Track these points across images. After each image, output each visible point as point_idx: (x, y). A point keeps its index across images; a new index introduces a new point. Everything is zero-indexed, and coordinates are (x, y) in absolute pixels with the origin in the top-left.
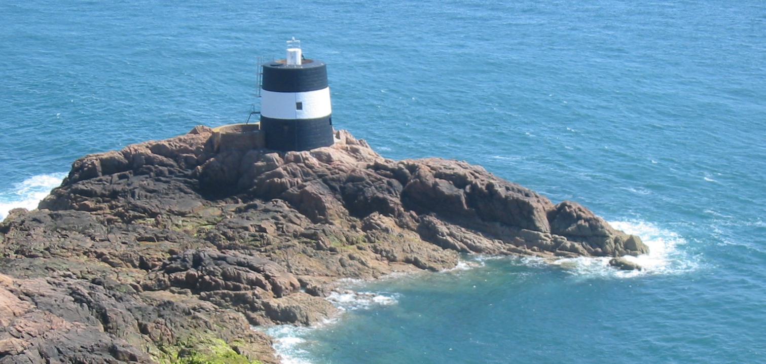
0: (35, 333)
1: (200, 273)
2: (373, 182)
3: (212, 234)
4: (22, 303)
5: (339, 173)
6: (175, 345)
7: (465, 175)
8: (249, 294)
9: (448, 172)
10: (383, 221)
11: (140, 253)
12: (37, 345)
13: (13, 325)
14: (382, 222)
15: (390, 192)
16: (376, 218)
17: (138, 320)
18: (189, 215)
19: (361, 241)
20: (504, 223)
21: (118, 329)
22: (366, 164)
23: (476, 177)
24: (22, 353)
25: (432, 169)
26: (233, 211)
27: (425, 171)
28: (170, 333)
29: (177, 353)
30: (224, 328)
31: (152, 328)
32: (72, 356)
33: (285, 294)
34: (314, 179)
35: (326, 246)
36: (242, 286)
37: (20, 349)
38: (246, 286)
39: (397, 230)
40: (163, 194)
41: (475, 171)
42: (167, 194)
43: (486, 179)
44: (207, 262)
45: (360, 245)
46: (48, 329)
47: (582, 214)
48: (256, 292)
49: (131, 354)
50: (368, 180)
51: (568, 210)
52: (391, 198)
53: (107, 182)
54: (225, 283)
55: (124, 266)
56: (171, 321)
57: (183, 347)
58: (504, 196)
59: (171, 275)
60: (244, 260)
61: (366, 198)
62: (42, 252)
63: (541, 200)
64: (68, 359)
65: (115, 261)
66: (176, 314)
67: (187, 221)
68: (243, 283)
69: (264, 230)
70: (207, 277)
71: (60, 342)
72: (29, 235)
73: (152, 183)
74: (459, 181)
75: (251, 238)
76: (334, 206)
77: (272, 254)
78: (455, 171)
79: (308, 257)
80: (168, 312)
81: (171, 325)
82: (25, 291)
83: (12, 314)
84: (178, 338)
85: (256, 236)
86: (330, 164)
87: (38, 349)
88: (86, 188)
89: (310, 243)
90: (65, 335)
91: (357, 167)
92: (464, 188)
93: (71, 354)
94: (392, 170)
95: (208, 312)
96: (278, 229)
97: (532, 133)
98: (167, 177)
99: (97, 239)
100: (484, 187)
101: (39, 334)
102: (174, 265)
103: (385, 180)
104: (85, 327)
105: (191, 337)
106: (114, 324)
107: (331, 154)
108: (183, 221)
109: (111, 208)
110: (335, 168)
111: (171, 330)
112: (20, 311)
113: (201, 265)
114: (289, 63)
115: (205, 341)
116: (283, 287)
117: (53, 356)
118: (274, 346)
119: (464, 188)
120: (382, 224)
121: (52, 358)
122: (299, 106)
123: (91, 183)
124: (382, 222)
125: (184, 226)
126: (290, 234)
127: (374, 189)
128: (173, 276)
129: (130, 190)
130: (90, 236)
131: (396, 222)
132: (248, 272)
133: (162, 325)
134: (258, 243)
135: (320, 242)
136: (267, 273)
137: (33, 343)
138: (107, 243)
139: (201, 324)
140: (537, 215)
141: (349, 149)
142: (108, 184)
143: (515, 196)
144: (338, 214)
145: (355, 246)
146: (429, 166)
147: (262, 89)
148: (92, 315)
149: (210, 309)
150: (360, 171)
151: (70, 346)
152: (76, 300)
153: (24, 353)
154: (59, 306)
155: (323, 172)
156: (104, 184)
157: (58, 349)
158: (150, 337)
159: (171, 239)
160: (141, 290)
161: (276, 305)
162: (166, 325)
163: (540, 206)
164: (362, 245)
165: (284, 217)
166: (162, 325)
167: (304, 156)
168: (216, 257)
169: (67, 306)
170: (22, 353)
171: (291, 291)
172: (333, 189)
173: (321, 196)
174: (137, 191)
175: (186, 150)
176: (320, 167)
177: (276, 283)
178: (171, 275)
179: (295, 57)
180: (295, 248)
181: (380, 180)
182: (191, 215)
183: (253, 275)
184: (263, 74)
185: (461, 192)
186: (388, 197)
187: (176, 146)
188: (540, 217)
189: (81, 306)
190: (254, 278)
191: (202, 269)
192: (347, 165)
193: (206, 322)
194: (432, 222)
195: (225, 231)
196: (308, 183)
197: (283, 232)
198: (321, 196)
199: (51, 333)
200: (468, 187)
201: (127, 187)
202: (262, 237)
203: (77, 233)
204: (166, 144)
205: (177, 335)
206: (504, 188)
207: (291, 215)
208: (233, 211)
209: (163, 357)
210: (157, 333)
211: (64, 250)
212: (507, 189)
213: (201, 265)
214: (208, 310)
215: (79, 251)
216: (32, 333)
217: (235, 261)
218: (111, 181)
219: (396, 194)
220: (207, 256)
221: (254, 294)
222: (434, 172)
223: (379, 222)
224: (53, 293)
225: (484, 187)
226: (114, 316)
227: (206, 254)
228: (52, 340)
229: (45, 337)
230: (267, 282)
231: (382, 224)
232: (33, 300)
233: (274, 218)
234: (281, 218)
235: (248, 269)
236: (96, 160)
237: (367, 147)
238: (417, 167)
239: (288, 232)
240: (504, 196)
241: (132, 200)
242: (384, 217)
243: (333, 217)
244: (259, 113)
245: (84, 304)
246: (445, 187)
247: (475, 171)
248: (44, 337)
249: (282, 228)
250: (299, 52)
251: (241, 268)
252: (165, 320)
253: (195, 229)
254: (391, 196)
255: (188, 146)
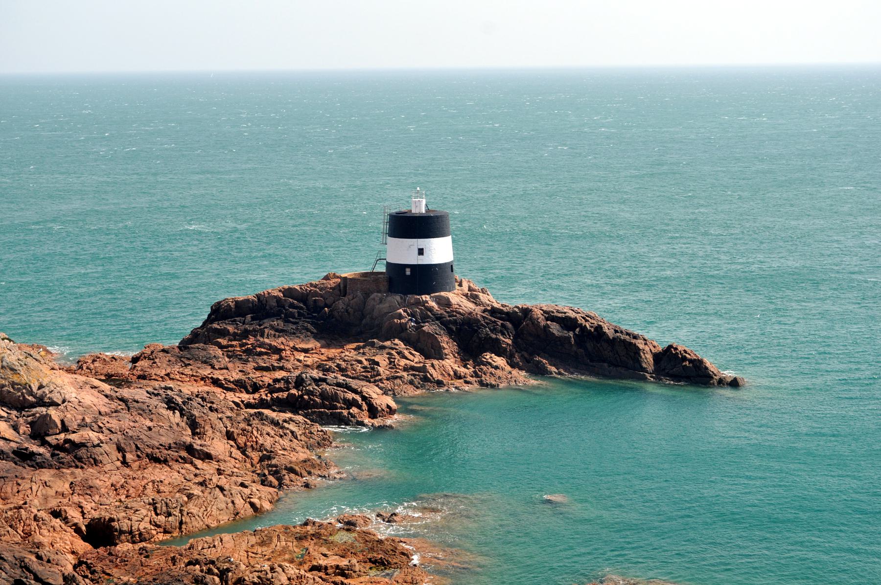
0: (116, 429)
1: (300, 393)
2: (487, 323)
3: (327, 367)
4: (110, 404)
5: (456, 316)
6: (258, 451)
7: (576, 317)
8: (345, 412)
9: (560, 315)
10: (494, 359)
11: (254, 380)
12: (116, 440)
13: (96, 422)
14: (494, 361)
15: (503, 334)
16: (488, 357)
17: (226, 427)
18: (311, 352)
19: (468, 376)
20: (611, 364)
21: (204, 434)
22: (483, 308)
23: (586, 321)
24: (98, 445)
25: (545, 312)
26: (353, 349)
27: (538, 313)
28: (255, 440)
29: (259, 458)
30: (311, 439)
31: (238, 434)
32: (149, 452)
33: (381, 414)
34: (433, 321)
35: (433, 378)
36: (339, 405)
37: (96, 442)
38: (343, 405)
39: (508, 368)
40: (291, 333)
41: (586, 316)
42: (294, 333)
43: (596, 323)
44: (309, 382)
45: (468, 379)
46: (130, 427)
47: (687, 356)
48: (351, 411)
49: (207, 452)
50: (483, 322)
51: (674, 352)
52: (504, 339)
53: (240, 322)
54: (323, 402)
55: (238, 391)
56: (258, 429)
57: (265, 452)
58: (611, 338)
59: (273, 395)
60: (343, 382)
61: (480, 339)
62: (162, 377)
63: (648, 343)
64: (144, 455)
65: (229, 386)
66: (264, 423)
67: (309, 357)
68: (340, 403)
69: (378, 364)
70: (306, 397)
71: (140, 439)
72: (155, 363)
73: (281, 323)
74: (568, 323)
75: (362, 370)
76: (449, 346)
77: (380, 384)
78: (567, 314)
79: (415, 388)
80: (257, 422)
81: (258, 433)
82: (120, 397)
83: (98, 413)
84: (262, 445)
85: (367, 368)
86: (449, 308)
87: (116, 444)
88: (219, 327)
89: (418, 375)
90: (146, 433)
91: (474, 310)
92: (574, 331)
93: (149, 451)
94: (508, 314)
95: (297, 423)
96: (391, 363)
97: (454, 110)
98: (296, 319)
99: (217, 367)
100: (592, 330)
101: (120, 431)
102: (277, 386)
103: (500, 322)
104: (168, 428)
105: (274, 444)
106: (202, 430)
107: (450, 298)
108: (305, 357)
109: (241, 346)
110: (453, 311)
111: (256, 437)
112: (106, 410)
113: (302, 385)
114: (415, 211)
115: (288, 448)
116: (379, 408)
117: (131, 452)
118: (453, 527)
119: (574, 331)
120: (493, 363)
121: (128, 453)
122: (421, 252)
123: (225, 323)
124: (494, 361)
125: (305, 361)
126: (400, 367)
127: (488, 330)
128: (275, 395)
129: (260, 329)
130: (211, 365)
131: (507, 362)
132: (347, 392)
133: (248, 432)
134: (369, 375)
135: (428, 374)
136: (364, 394)
137: (112, 438)
138: (225, 371)
139: (288, 433)
140: (643, 357)
141: (469, 295)
142: (241, 324)
143: (622, 338)
144: (453, 354)
145: (462, 381)
146: (542, 310)
147: (387, 237)
148: (182, 421)
149: (300, 422)
150: (477, 314)
151: (148, 443)
152: (169, 408)
153: (101, 447)
154: (150, 411)
155: (441, 314)
156: (237, 324)
157: (136, 446)
158: (235, 443)
159: (286, 369)
160: (244, 408)
161: (371, 424)
162: (252, 432)
163: (647, 349)
164: (469, 379)
165: (399, 353)
166: (248, 432)
167: (424, 299)
168: (318, 378)
169: (159, 412)
170: (98, 445)
171: (387, 412)
172: (450, 333)
173: (437, 336)
174: (266, 331)
175: (315, 294)
176: (439, 309)
177: (373, 404)
178: (273, 395)
179: (420, 207)
180: (403, 379)
181: (495, 322)
182: (314, 351)
183: (350, 396)
184: (389, 222)
185: (571, 334)
186: (501, 338)
187: (306, 290)
188: (646, 358)
189: (174, 413)
190: (351, 398)
191: (303, 389)
192: (465, 309)
193: (292, 432)
194: (542, 362)
195: (340, 363)
196: (427, 324)
197: (395, 365)
198: (437, 336)
199: (132, 430)
200: (578, 330)
201: (258, 327)
202: (373, 369)
203: (200, 362)
204: (298, 288)
205: (260, 442)
206: (613, 331)
207: (406, 353)
208: (353, 349)
209: (245, 461)
210: (241, 440)
211: (184, 376)
212: (616, 331)
213: (302, 385)
214: (298, 422)
215: (197, 376)
216: (113, 430)
217: (335, 382)
218: (244, 321)
219: (510, 336)
220: (308, 377)
221: (349, 413)
222: (547, 316)
223: (490, 361)
224: (148, 400)
225: (592, 330)
226: (203, 423)
227: (308, 375)
228: (131, 437)
229: (126, 434)
230: (364, 403)
231: (493, 363)
232: (126, 405)
233: (389, 354)
234: (396, 354)
235: (345, 390)
236: (232, 302)
237: (488, 295)
238: (531, 310)
239: (399, 365)
240: (611, 338)
241: (261, 339)
242: (496, 357)
243: (448, 357)
244: (385, 259)
245: (176, 411)
246: (555, 328)
247: (586, 316)
248: (124, 434)
249: (394, 362)
250: (424, 202)
251: (339, 389)
252: (252, 429)
253: (315, 364)
254: (504, 337)
255: (318, 290)
